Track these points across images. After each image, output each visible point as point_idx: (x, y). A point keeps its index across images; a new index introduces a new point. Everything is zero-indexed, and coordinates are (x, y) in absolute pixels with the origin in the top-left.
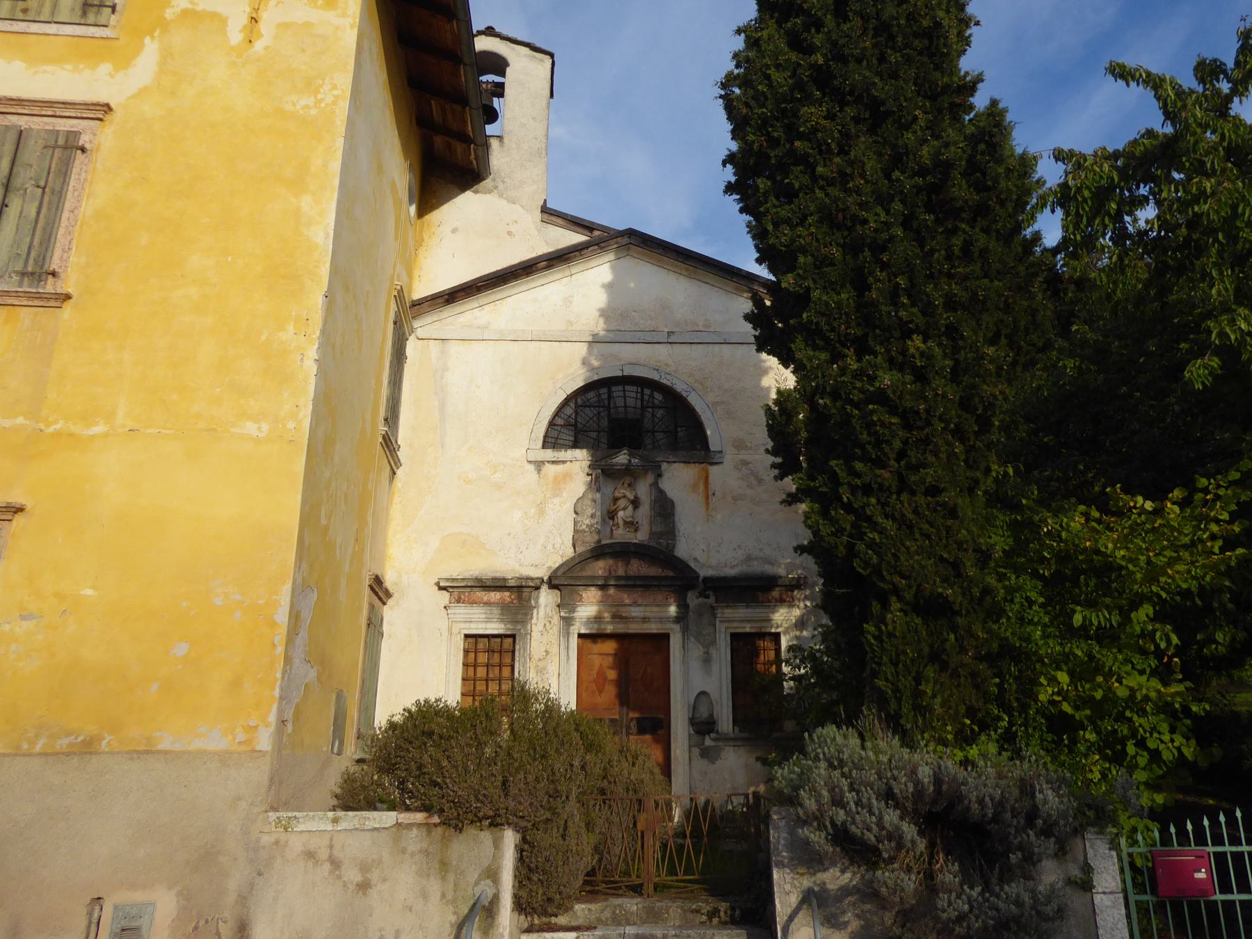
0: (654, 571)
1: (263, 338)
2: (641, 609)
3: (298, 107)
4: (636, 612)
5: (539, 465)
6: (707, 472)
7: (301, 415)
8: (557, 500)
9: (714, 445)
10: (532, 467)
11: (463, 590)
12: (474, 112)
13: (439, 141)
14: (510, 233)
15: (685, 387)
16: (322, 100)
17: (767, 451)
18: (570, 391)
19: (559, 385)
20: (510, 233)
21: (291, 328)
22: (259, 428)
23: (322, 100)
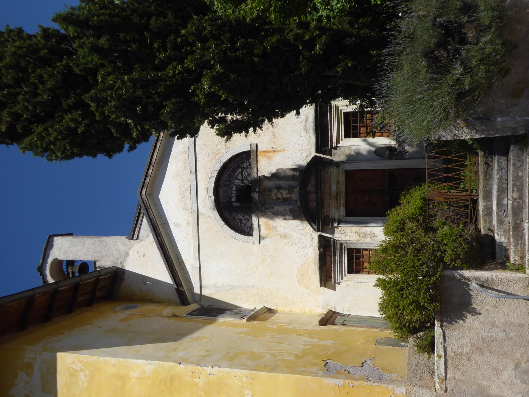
0: (313, 179)
1: (202, 394)
2: (332, 185)
3: (85, 380)
4: (334, 188)
5: (260, 238)
6: (261, 152)
7: (239, 374)
8: (279, 228)
9: (247, 148)
10: (262, 242)
11: (327, 278)
12: (82, 279)
13: (98, 294)
14: (144, 255)
15: (218, 164)
16: (81, 368)
17: (246, 136)
18: (223, 223)
19: (220, 229)
20: (144, 255)
21: (197, 380)
22: (248, 395)
23: (81, 368)
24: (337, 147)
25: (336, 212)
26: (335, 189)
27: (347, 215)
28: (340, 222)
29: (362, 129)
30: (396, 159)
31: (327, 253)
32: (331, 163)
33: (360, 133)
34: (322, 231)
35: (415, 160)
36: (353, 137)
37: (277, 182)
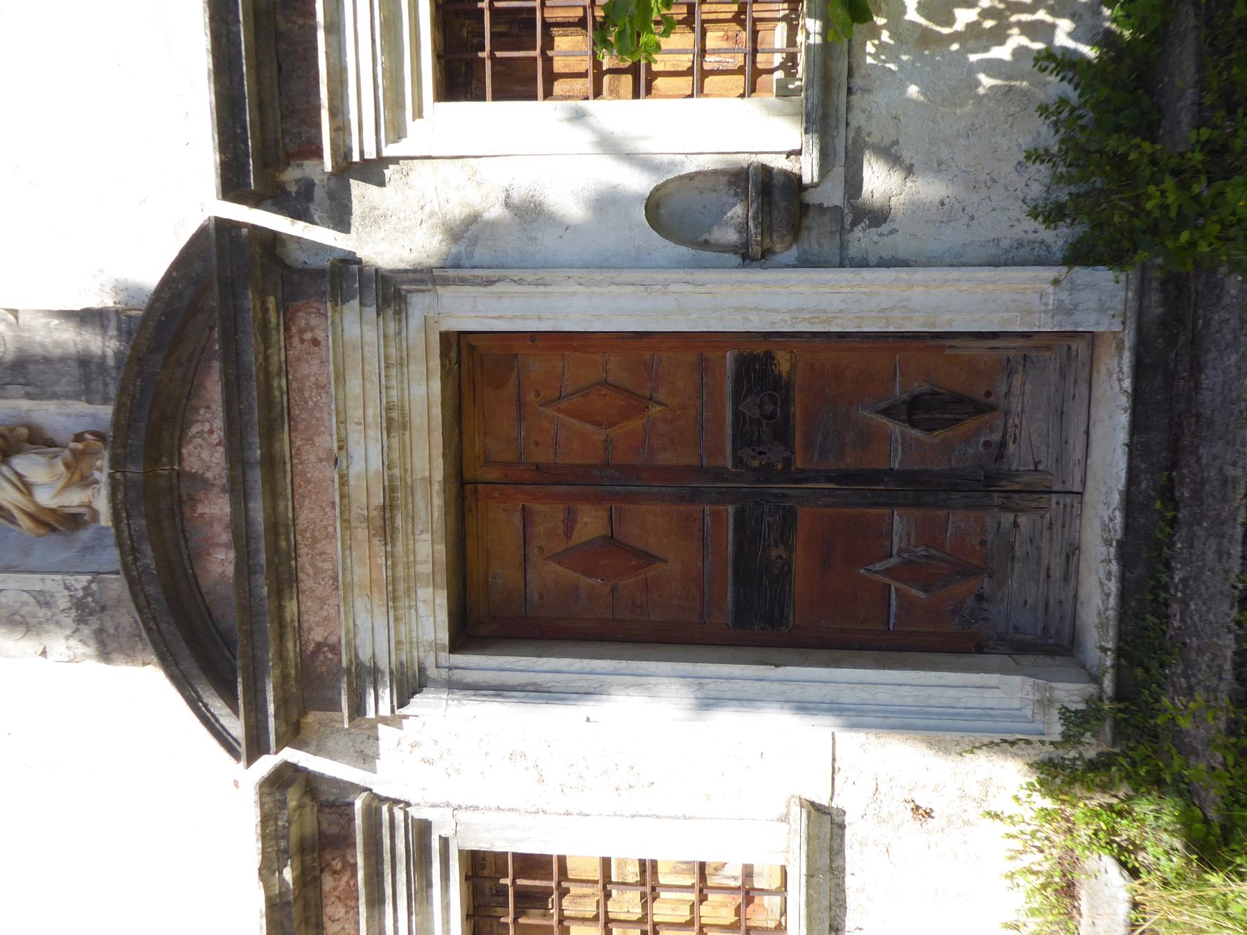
2: (355, 436)
4: (366, 457)
24: (383, 162)
25: (380, 623)
26: (376, 463)
27: (468, 631)
28: (409, 686)
29: (563, 42)
30: (805, 263)
31: (328, 882)
32: (344, 276)
33: (551, 77)
34: (293, 735)
35: (935, 274)
36: (501, 94)
37: (25, 405)
